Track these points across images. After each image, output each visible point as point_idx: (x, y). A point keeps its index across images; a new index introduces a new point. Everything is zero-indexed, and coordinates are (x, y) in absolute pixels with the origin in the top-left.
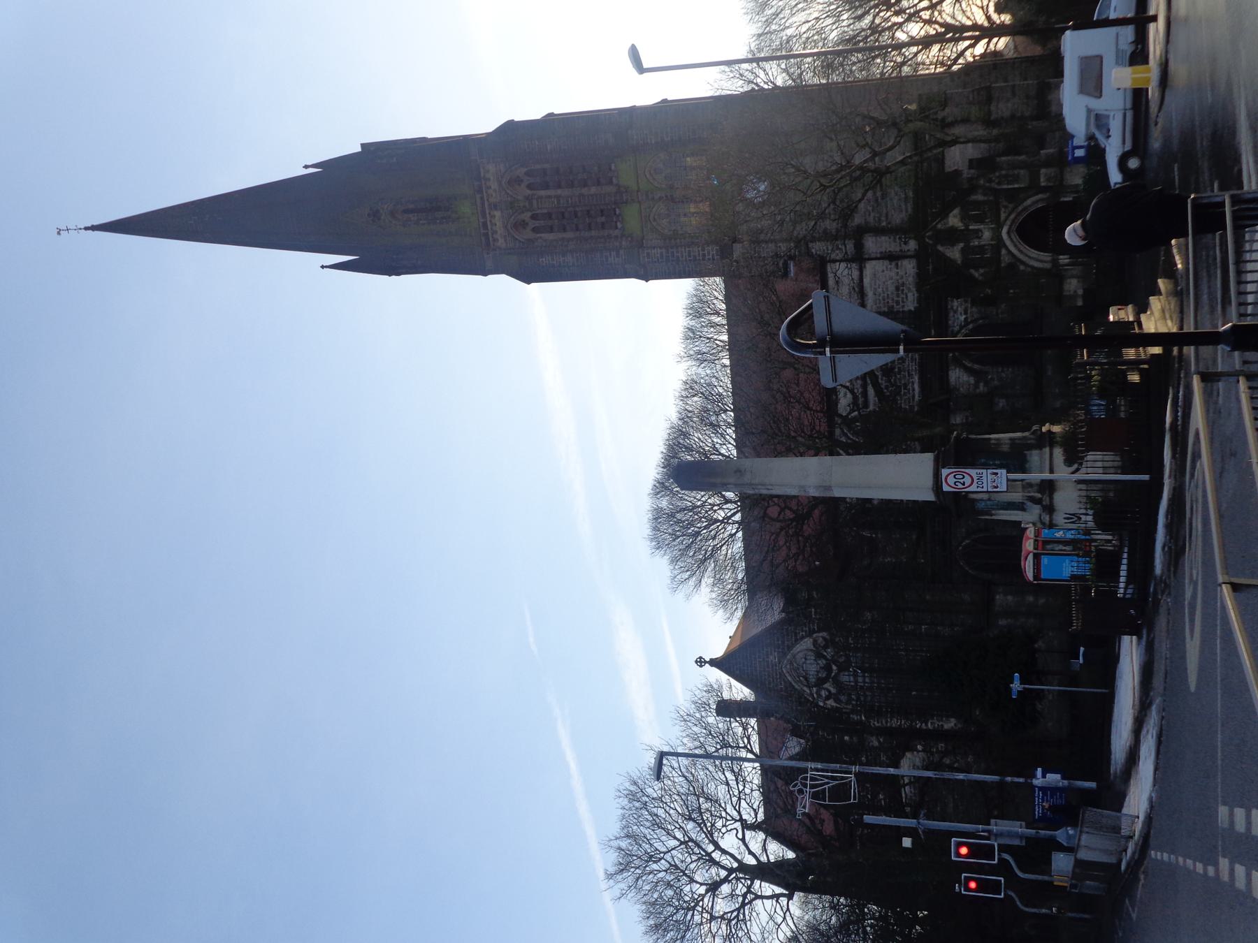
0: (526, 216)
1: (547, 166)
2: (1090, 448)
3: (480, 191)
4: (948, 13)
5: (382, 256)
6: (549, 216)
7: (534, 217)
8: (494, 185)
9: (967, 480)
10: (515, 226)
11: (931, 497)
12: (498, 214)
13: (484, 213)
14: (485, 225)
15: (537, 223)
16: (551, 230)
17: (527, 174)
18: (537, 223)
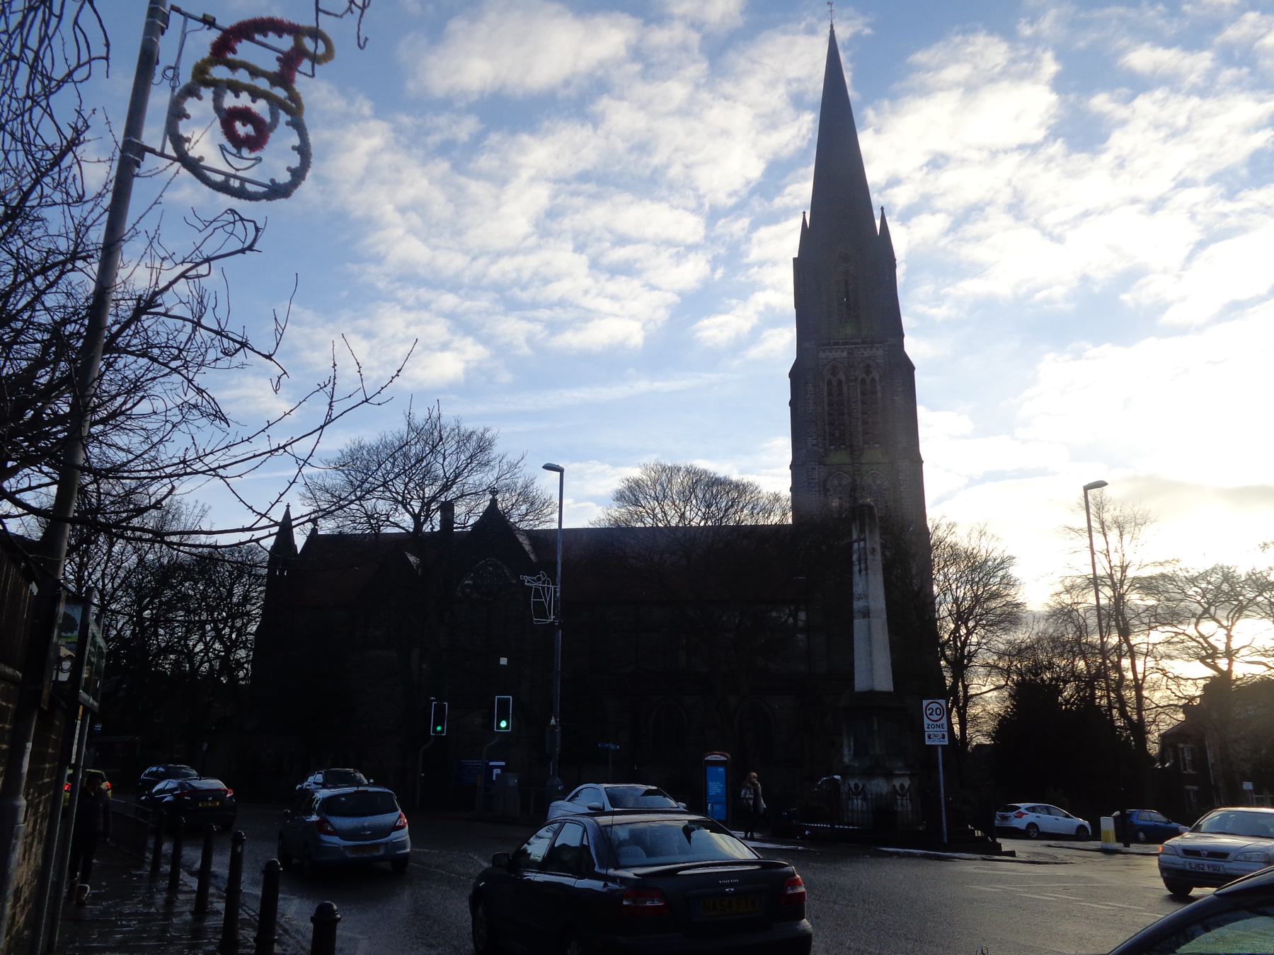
0: (842, 377)
1: (879, 395)
2: (584, 848)
3: (863, 342)
4: (1135, 888)
5: (809, 271)
6: (841, 394)
7: (840, 382)
8: (866, 354)
9: (935, 717)
10: (868, 366)
11: (1234, 677)
12: (845, 354)
13: (846, 343)
14: (837, 344)
15: (835, 384)
16: (830, 394)
17: (873, 380)
18: (868, 382)
